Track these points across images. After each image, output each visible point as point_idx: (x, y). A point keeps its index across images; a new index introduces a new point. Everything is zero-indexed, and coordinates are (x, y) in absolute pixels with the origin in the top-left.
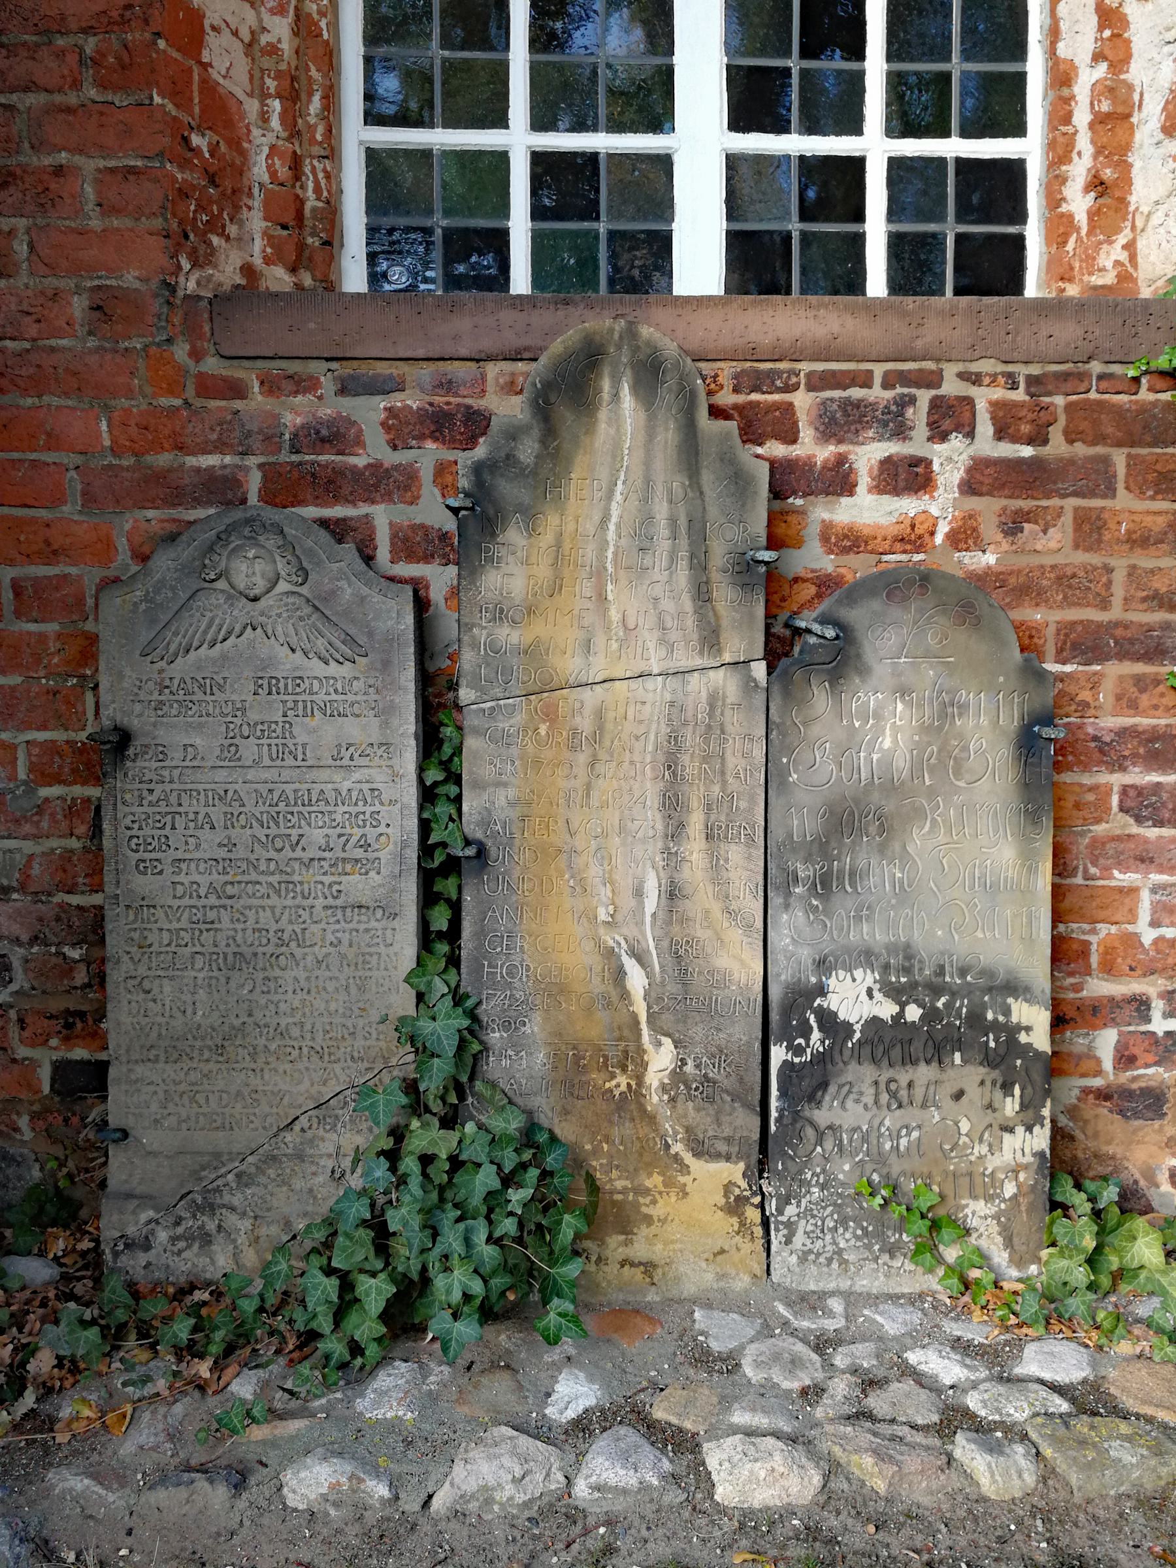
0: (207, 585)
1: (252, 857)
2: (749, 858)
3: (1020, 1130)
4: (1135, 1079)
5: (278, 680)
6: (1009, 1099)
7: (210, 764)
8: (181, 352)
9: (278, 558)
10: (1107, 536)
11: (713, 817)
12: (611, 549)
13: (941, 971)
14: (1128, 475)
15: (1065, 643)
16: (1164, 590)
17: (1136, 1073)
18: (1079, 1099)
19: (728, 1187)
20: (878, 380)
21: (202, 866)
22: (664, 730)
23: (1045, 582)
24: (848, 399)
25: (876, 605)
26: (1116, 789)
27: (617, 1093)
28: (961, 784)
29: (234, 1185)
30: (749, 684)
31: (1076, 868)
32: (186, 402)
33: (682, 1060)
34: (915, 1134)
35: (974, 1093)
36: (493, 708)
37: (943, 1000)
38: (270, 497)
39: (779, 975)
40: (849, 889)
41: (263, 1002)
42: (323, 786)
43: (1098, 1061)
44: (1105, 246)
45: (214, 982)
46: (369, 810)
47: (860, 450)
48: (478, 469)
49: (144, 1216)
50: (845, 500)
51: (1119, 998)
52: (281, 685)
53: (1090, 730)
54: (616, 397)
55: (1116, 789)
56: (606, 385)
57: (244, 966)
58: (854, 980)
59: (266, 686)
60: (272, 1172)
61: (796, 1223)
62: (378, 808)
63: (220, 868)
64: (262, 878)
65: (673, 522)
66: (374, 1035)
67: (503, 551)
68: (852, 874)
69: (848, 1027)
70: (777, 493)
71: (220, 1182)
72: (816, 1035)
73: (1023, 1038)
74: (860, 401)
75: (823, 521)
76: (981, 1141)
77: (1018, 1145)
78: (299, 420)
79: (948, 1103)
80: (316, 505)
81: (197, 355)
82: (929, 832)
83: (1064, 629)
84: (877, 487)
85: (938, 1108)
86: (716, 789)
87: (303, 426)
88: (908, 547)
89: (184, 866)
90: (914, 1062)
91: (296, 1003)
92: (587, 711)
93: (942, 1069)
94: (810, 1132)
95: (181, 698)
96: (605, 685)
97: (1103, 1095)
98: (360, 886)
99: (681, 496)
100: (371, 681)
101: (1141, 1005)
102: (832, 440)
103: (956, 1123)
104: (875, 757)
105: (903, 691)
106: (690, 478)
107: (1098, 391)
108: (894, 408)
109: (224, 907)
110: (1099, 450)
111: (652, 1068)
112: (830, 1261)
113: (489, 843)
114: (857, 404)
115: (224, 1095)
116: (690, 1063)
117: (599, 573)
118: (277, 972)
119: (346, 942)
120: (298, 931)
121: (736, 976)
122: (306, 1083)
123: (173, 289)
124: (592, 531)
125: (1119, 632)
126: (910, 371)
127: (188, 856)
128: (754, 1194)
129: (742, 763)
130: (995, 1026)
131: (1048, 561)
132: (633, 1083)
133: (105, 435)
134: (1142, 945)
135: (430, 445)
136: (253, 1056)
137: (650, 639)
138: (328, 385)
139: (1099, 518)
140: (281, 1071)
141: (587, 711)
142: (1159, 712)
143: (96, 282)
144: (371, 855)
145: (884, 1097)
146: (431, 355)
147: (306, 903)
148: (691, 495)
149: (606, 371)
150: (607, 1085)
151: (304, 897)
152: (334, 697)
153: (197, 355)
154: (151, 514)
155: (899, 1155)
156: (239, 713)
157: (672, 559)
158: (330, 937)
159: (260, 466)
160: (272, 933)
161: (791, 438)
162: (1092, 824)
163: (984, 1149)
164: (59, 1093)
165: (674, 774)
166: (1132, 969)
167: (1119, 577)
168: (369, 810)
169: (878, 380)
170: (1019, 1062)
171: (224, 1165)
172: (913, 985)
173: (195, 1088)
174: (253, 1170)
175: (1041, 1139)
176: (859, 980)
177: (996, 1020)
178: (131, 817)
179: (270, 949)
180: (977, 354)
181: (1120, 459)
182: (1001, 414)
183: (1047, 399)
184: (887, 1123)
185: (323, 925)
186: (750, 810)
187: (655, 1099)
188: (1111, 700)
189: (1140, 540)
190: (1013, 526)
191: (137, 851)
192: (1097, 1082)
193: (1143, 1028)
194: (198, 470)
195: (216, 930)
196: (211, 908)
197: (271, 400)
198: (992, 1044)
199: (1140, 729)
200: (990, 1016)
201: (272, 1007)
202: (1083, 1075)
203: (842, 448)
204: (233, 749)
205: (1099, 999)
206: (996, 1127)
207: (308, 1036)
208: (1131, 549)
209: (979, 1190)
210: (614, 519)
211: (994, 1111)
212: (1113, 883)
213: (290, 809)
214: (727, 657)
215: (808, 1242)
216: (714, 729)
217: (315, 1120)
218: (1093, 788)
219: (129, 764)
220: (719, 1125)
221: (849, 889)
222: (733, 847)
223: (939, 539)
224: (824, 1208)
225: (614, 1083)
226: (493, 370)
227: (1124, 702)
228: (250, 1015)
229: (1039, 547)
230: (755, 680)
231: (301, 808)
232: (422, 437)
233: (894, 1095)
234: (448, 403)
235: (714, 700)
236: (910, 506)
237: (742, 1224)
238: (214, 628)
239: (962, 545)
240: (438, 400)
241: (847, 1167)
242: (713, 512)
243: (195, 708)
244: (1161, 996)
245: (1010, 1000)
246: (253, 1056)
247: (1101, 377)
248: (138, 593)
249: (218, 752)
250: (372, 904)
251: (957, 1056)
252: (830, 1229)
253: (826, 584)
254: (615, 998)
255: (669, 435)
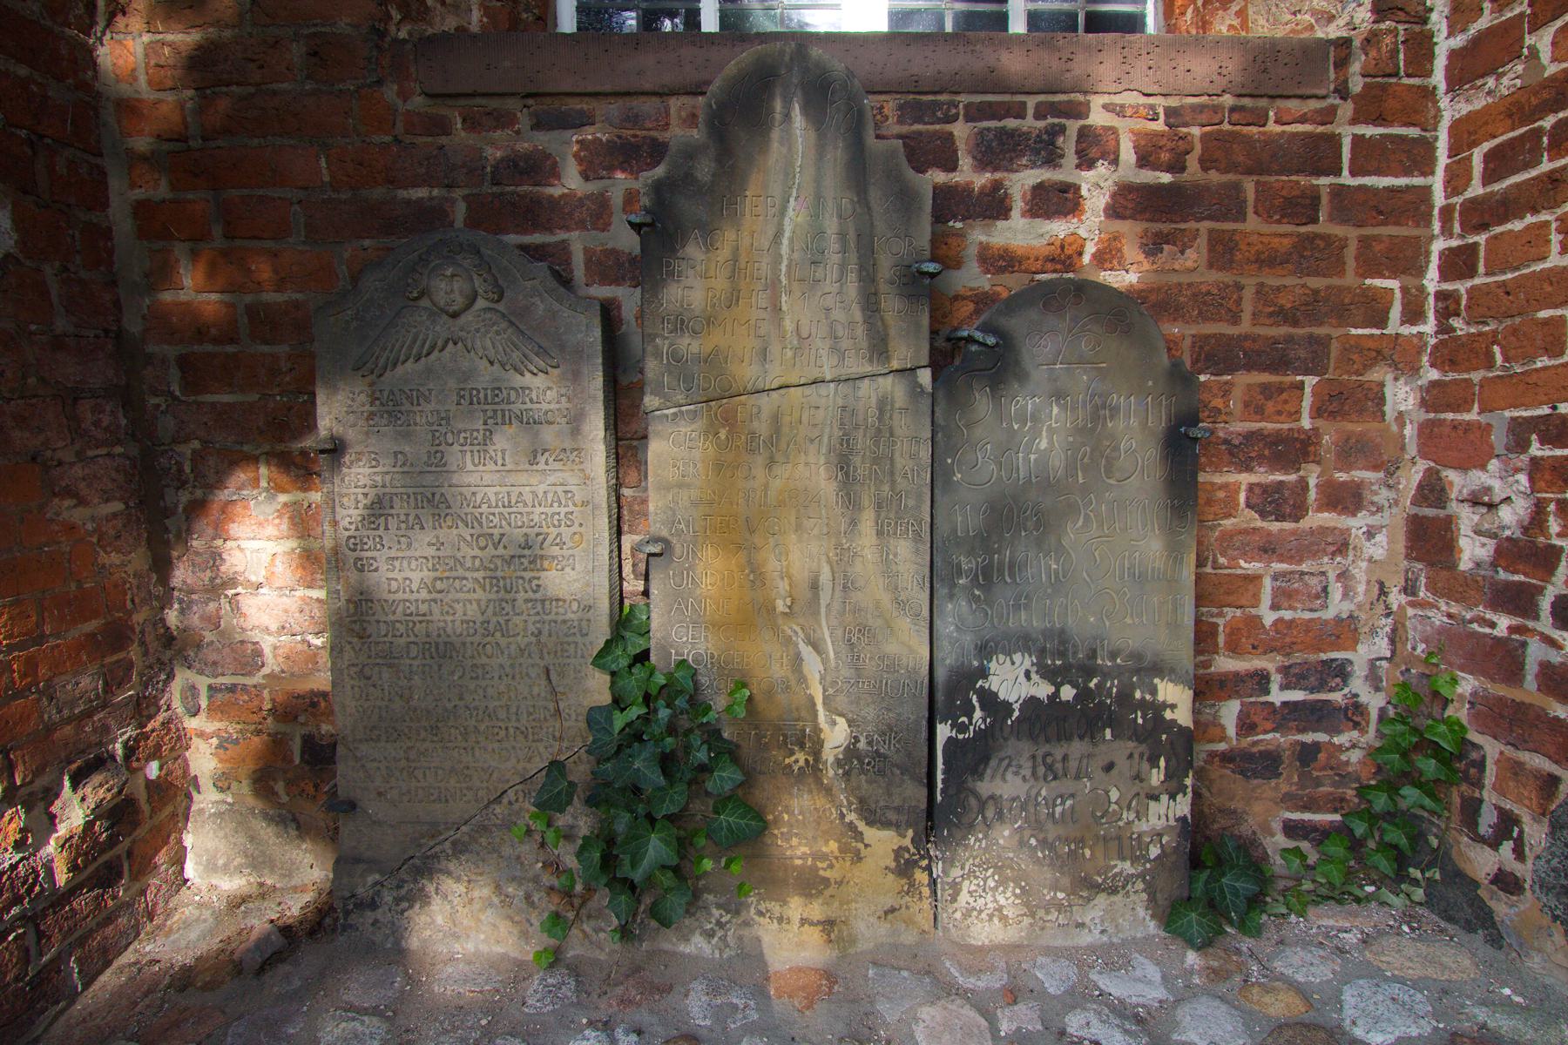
0: (411, 303)
1: (459, 555)
2: (917, 551)
3: (1164, 798)
4: (1255, 743)
5: (478, 391)
6: (1155, 771)
7: (418, 469)
8: (390, 92)
9: (475, 277)
10: (1238, 256)
11: (883, 515)
12: (785, 263)
13: (1093, 654)
14: (1257, 200)
15: (1199, 355)
16: (1289, 306)
17: (1255, 738)
18: (1205, 762)
19: (898, 853)
20: (1030, 111)
21: (413, 565)
22: (837, 433)
23: (1182, 299)
24: (1003, 128)
25: (1033, 314)
26: (1243, 487)
27: (796, 768)
28: (1112, 482)
29: (450, 852)
30: (915, 390)
31: (1207, 558)
32: (397, 140)
33: (855, 737)
34: (1069, 803)
35: (1122, 765)
36: (675, 414)
37: (1095, 681)
38: (473, 222)
39: (944, 660)
40: (1009, 580)
41: (472, 687)
42: (521, 489)
43: (1223, 728)
44: (1220, 12)
45: (427, 668)
46: (563, 510)
47: (1015, 176)
48: (658, 187)
49: (370, 880)
50: (1001, 224)
51: (1243, 673)
52: (482, 395)
53: (1221, 434)
54: (787, 116)
55: (1243, 487)
56: (778, 105)
57: (454, 654)
58: (1013, 663)
59: (467, 397)
60: (483, 841)
61: (960, 883)
62: (571, 508)
63: (430, 565)
64: (468, 574)
65: (842, 236)
66: (574, 717)
67: (684, 265)
68: (1011, 567)
69: (1007, 706)
70: (940, 217)
71: (437, 849)
72: (978, 714)
73: (1168, 715)
74: (1015, 130)
75: (981, 243)
76: (1129, 808)
77: (1162, 812)
78: (499, 154)
79: (1099, 775)
80: (517, 233)
81: (404, 95)
82: (1082, 527)
83: (1200, 342)
84: (1030, 210)
85: (1090, 779)
86: (886, 488)
87: (502, 159)
88: (1058, 267)
89: (397, 563)
90: (1069, 738)
91: (502, 688)
92: (765, 415)
93: (1095, 745)
94: (973, 801)
95: (390, 408)
96: (782, 391)
97: (1227, 758)
98: (557, 581)
99: (850, 212)
100: (563, 391)
101: (1261, 680)
102: (989, 168)
103: (1107, 792)
104: (1033, 457)
105: (1059, 395)
106: (858, 195)
107: (1230, 123)
108: (1045, 137)
109: (435, 601)
110: (1231, 177)
111: (827, 746)
112: (991, 917)
113: (674, 541)
114: (1012, 133)
115: (440, 772)
116: (863, 740)
117: (773, 286)
118: (484, 660)
119: (545, 632)
120: (502, 622)
121: (904, 661)
122: (514, 761)
123: (382, 34)
124: (766, 245)
125: (1247, 344)
126: (1060, 103)
127: (400, 554)
128: (922, 857)
129: (911, 463)
130: (1143, 704)
131: (1185, 279)
132: (811, 759)
133: (324, 172)
134: (1263, 626)
135: (620, 175)
136: (465, 735)
137: (822, 346)
138: (524, 120)
139: (1231, 239)
140: (490, 749)
141: (765, 415)
142: (1282, 418)
143: (313, 30)
144: (566, 552)
145: (1041, 770)
146: (617, 89)
147: (508, 596)
148: (859, 210)
149: (778, 91)
150: (787, 761)
151: (506, 591)
152: (529, 405)
153: (404, 95)
154: (367, 243)
155: (1055, 822)
156: (443, 422)
157: (843, 267)
158: (531, 628)
159: (465, 198)
160: (478, 624)
161: (951, 166)
162: (1222, 519)
163: (1132, 816)
164: (308, 763)
165: (847, 474)
166: (1254, 647)
167: (1248, 294)
168: (563, 510)
169: (1030, 111)
170: (1164, 737)
171: (441, 834)
172: (1066, 668)
173: (413, 765)
174: (466, 838)
175: (1183, 806)
176: (1018, 663)
177: (1143, 698)
178: (348, 519)
179: (477, 639)
180: (1121, 88)
181: (1249, 186)
182: (1143, 143)
183: (1184, 130)
184: (1044, 793)
185: (524, 617)
186: (918, 507)
187: (831, 773)
188: (1240, 406)
189: (1268, 261)
190: (1153, 246)
191: (355, 550)
192: (1222, 746)
193: (1263, 699)
194: (408, 202)
195: (428, 622)
196: (423, 602)
197: (473, 135)
198: (1140, 721)
199: (1266, 433)
200: (1138, 695)
201: (481, 692)
202: (1211, 741)
203: (998, 175)
204: (439, 455)
205: (1226, 674)
206: (1142, 795)
207: (514, 718)
208: (1260, 268)
209: (1127, 852)
210: (787, 234)
211: (1142, 781)
212: (1239, 572)
213: (492, 510)
214: (895, 365)
215: (971, 900)
216: (883, 432)
217: (521, 794)
218: (1225, 486)
219: (345, 470)
220: (890, 795)
221: (1009, 580)
222: (902, 542)
223: (1086, 259)
224: (986, 870)
225: (793, 758)
226: (674, 103)
227: (1251, 409)
228: (461, 699)
229: (1177, 267)
230: (921, 386)
231: (502, 510)
232: (611, 168)
233: (1050, 768)
234: (635, 136)
235: (883, 405)
236: (1059, 228)
237: (911, 885)
238: (418, 343)
239: (1108, 265)
240: (627, 133)
241: (1006, 833)
242: (880, 226)
243: (403, 418)
244: (1279, 670)
245: (1156, 681)
246: (465, 735)
247: (1233, 110)
248: (349, 312)
249: (426, 459)
250: (568, 598)
251: (1108, 733)
252: (991, 889)
253: (983, 300)
254: (793, 683)
255: (837, 154)
